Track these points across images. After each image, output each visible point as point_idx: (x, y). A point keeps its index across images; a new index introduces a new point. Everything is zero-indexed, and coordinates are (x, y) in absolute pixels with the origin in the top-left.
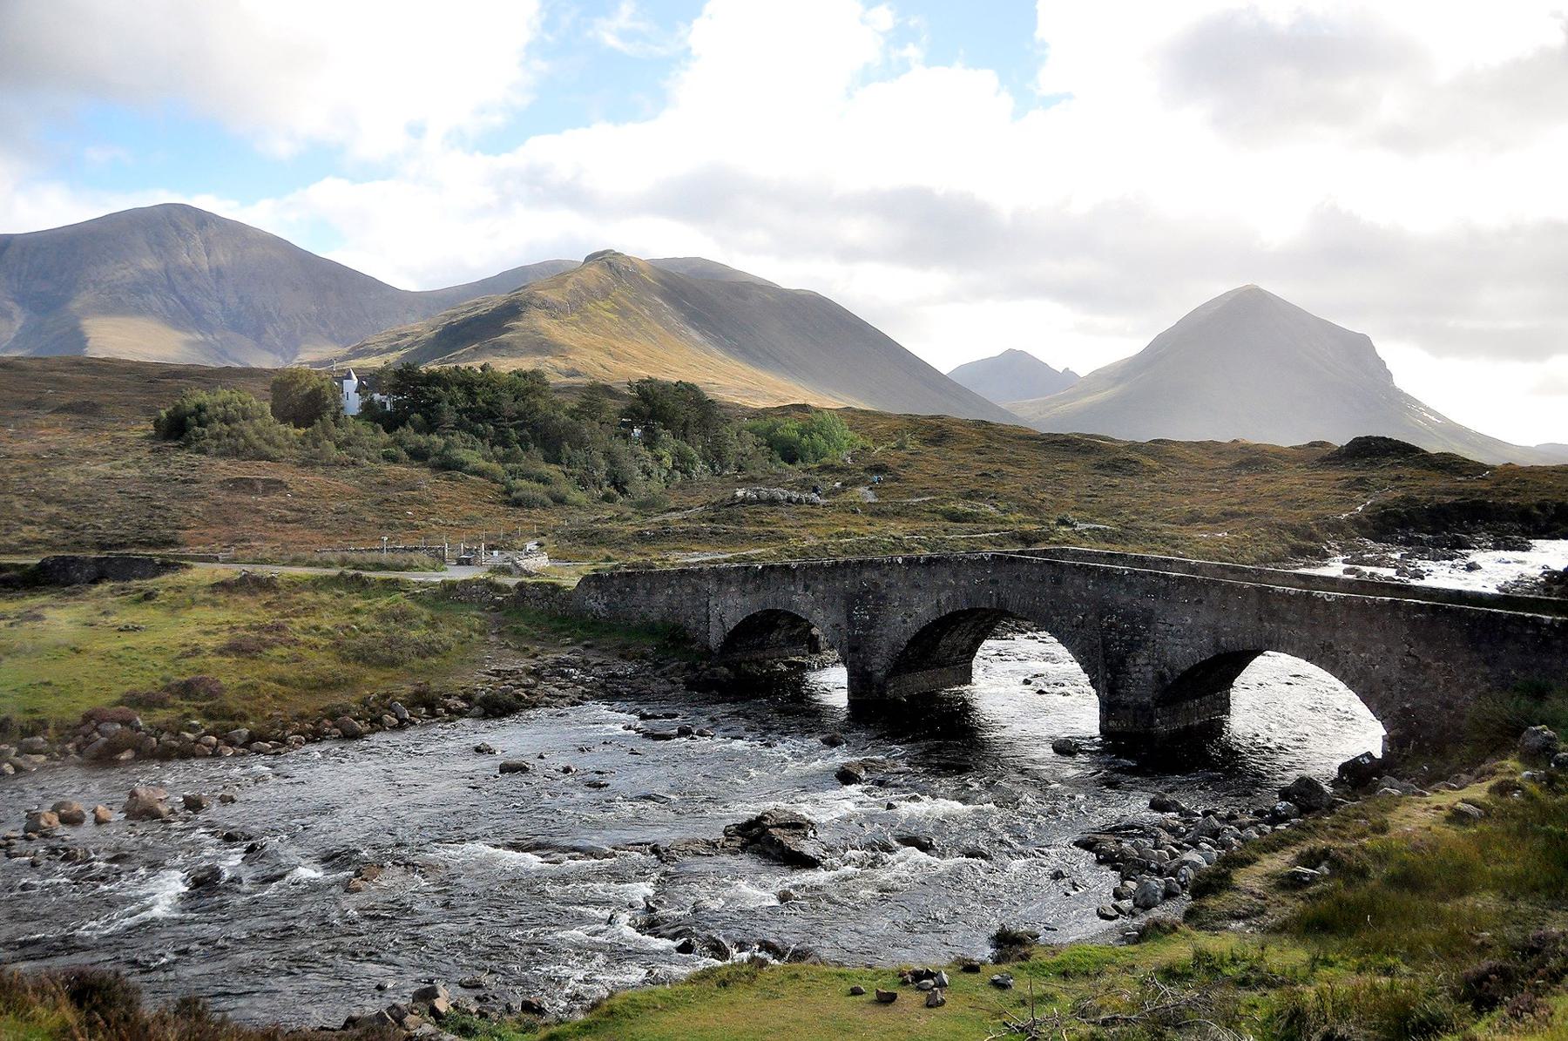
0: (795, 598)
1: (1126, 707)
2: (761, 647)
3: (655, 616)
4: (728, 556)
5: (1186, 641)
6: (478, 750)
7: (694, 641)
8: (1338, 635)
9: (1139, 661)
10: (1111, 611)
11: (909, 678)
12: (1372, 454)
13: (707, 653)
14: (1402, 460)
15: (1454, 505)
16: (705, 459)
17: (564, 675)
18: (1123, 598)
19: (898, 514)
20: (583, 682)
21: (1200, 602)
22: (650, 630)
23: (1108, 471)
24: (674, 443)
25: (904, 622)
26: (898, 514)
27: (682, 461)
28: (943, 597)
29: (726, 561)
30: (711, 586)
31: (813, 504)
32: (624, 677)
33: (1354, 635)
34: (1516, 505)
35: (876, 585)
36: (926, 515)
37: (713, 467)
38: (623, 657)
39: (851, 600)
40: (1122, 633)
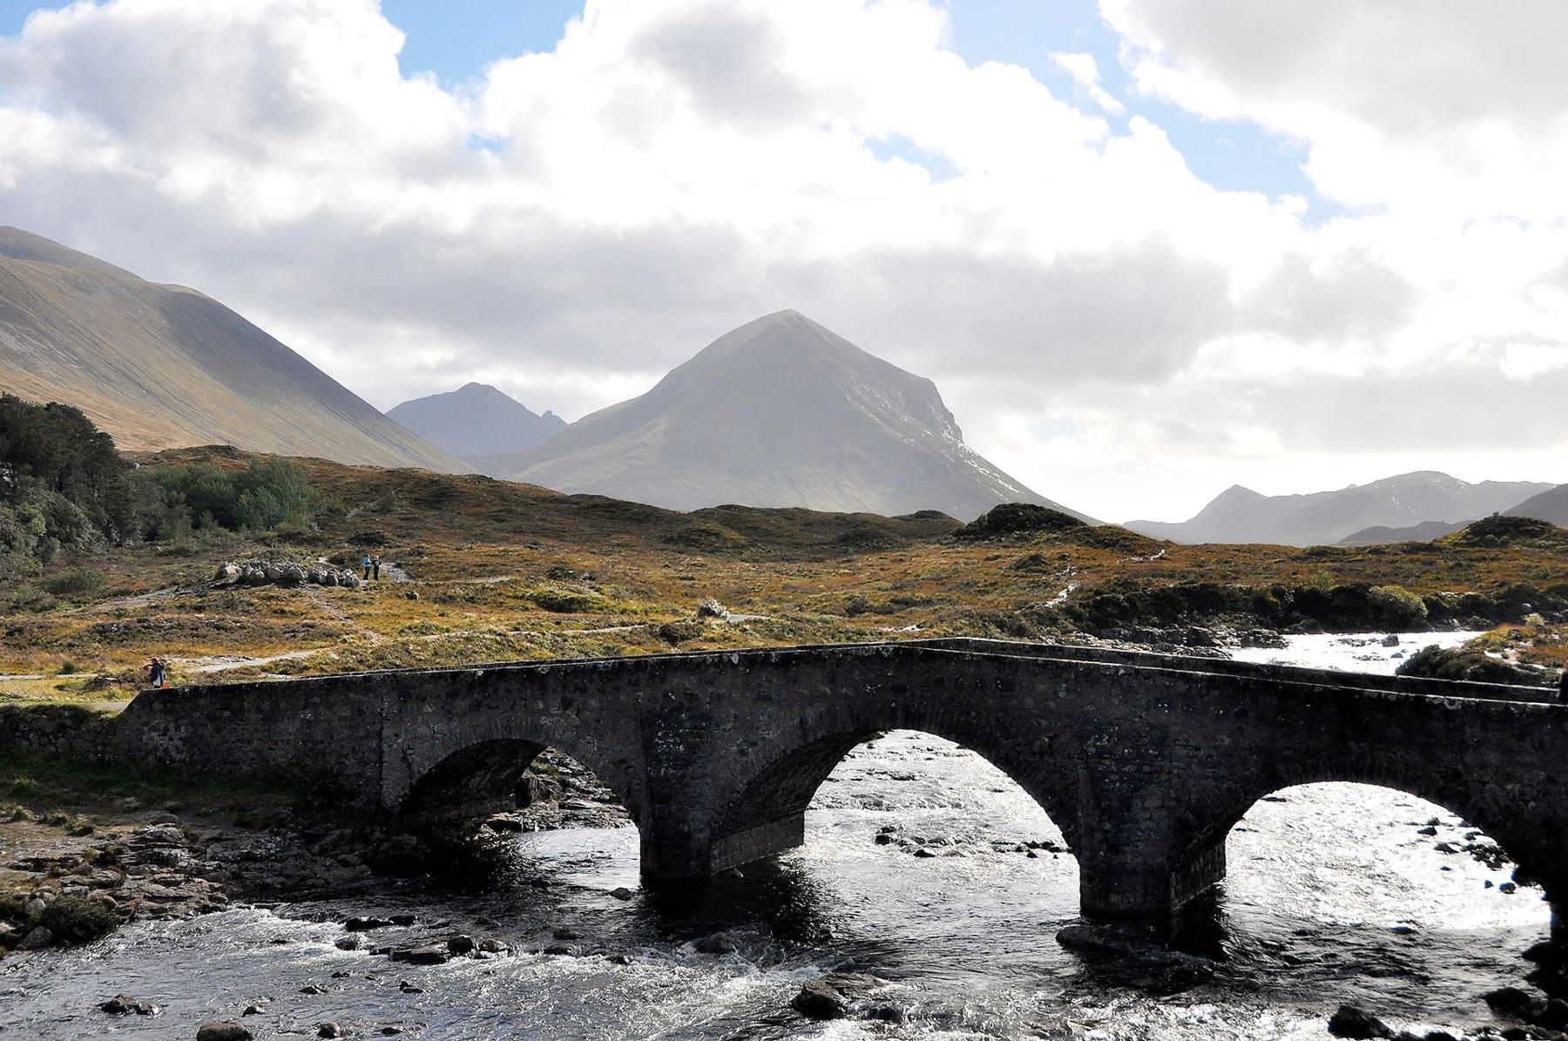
0: (544, 720)
1: (1133, 873)
2: (456, 801)
3: (280, 756)
4: (264, 662)
5: (1223, 771)
6: (112, 1009)
7: (353, 795)
8: (1469, 758)
9: (1148, 804)
10: (1099, 730)
11: (734, 840)
12: (1021, 527)
13: (379, 813)
14: (1058, 534)
15: (1181, 591)
16: (97, 522)
17: (163, 861)
18: (1118, 708)
19: (472, 600)
20: (200, 872)
21: (1243, 713)
22: (275, 779)
23: (681, 546)
24: (52, 496)
25: (743, 753)
26: (472, 600)
27: (61, 523)
28: (811, 715)
29: (264, 670)
30: (387, 704)
31: (349, 584)
32: (267, 858)
33: (1494, 758)
34: (1249, 591)
35: (692, 697)
36: (512, 603)
37: (108, 535)
38: (243, 824)
39: (647, 723)
40: (1123, 761)
